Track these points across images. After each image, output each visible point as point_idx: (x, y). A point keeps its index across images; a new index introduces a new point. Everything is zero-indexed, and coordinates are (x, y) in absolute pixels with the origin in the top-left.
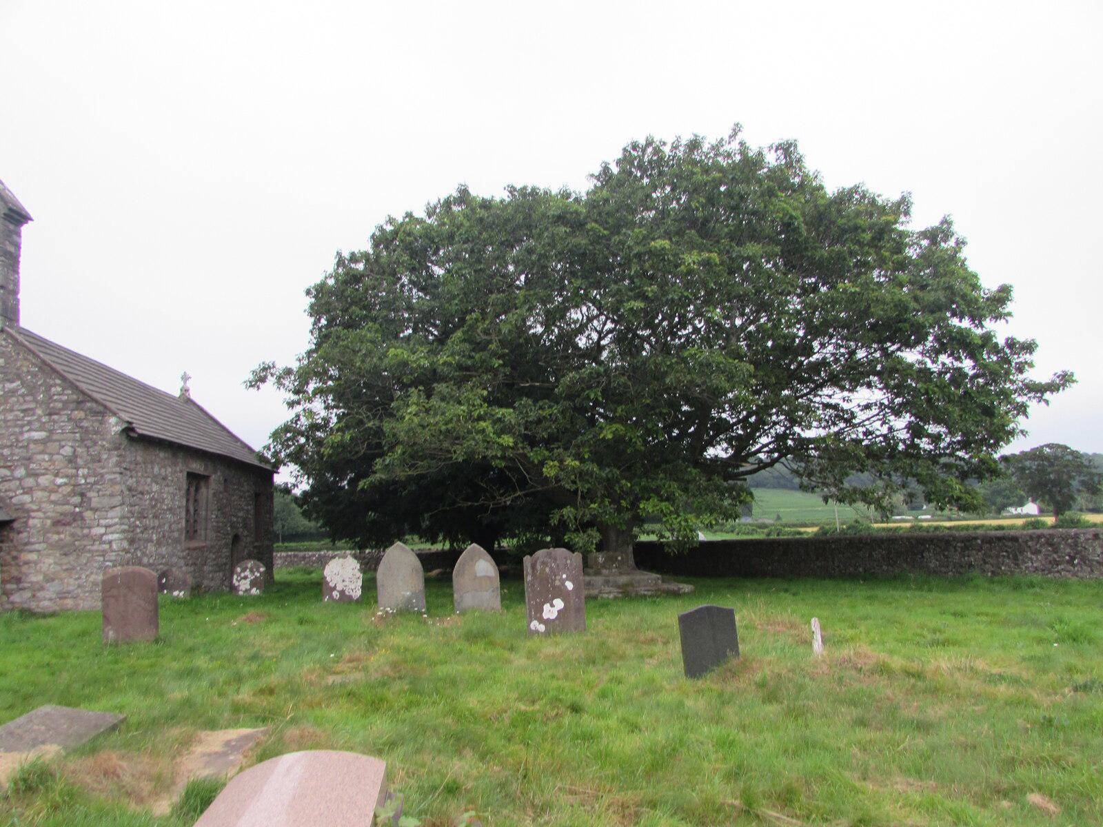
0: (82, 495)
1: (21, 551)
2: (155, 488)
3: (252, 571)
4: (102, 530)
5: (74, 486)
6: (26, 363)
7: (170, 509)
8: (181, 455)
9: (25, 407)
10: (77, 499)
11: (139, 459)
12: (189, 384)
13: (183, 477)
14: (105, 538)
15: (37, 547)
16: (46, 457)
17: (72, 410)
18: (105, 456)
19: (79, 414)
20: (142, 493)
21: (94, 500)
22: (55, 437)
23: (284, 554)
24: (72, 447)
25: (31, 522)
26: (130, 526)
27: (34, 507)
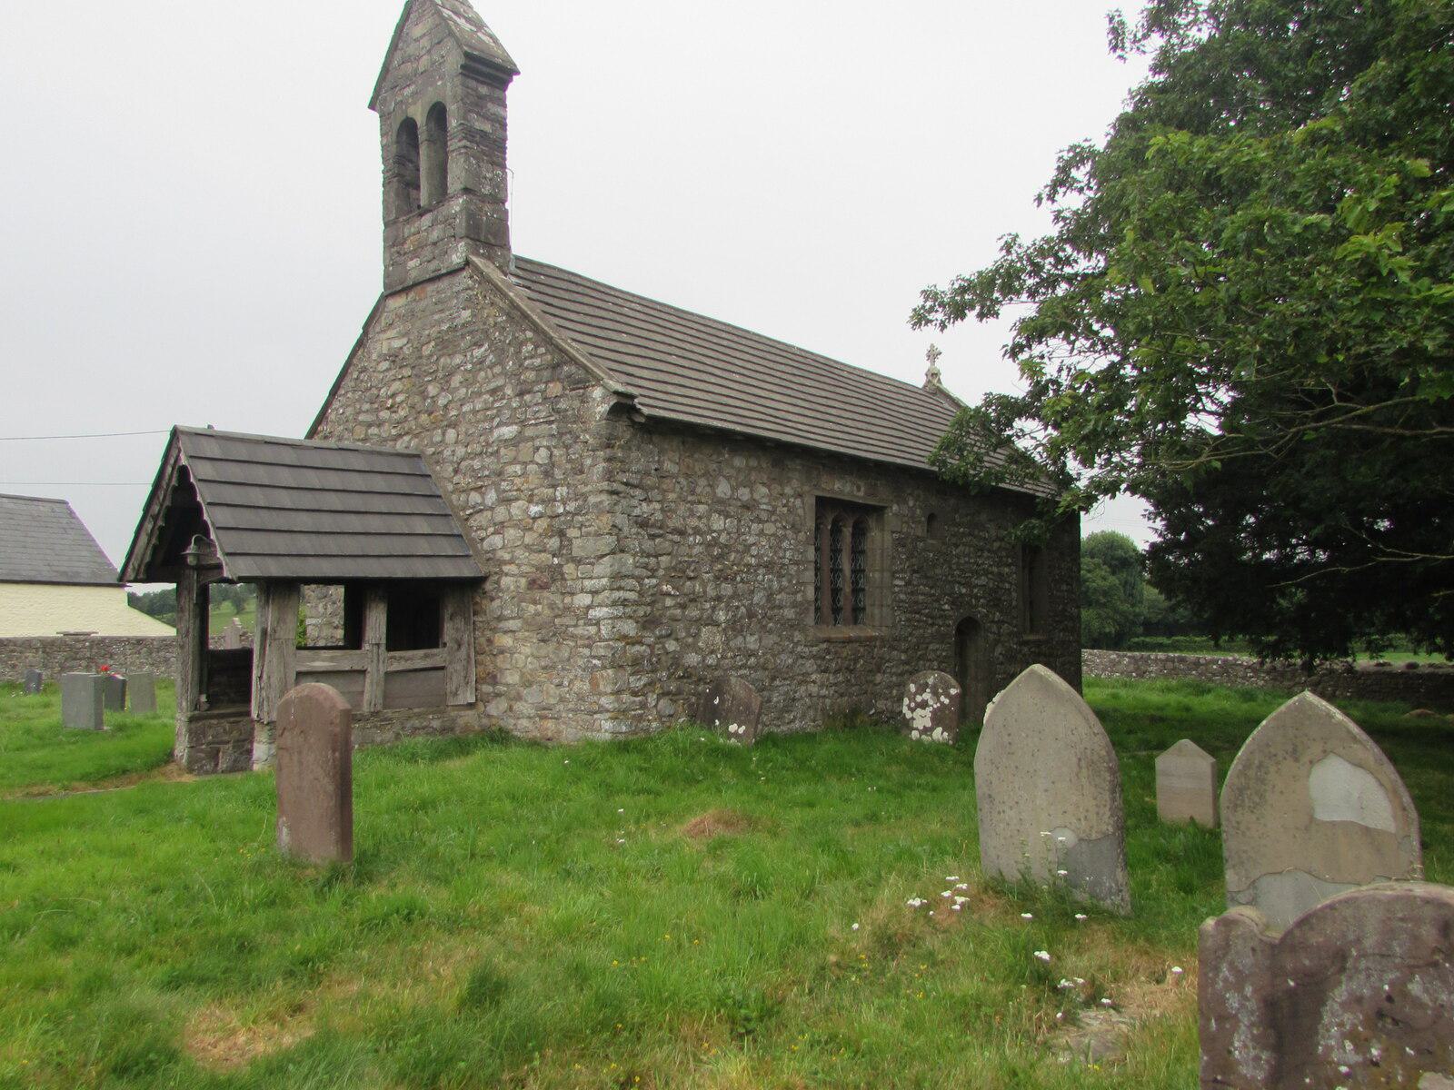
0: (562, 534)
1: (494, 630)
2: (718, 523)
3: (935, 694)
4: (587, 599)
5: (551, 517)
6: (494, 311)
7: (768, 566)
8: (796, 464)
9: (492, 385)
10: (554, 543)
11: (668, 466)
12: (940, 364)
13: (804, 510)
14: (593, 613)
15: (511, 624)
16: (518, 468)
17: (547, 383)
18: (589, 462)
19: (555, 389)
20: (682, 533)
21: (576, 543)
22: (529, 432)
23: (1161, 655)
24: (548, 448)
25: (505, 581)
26: (641, 594)
27: (507, 557)
